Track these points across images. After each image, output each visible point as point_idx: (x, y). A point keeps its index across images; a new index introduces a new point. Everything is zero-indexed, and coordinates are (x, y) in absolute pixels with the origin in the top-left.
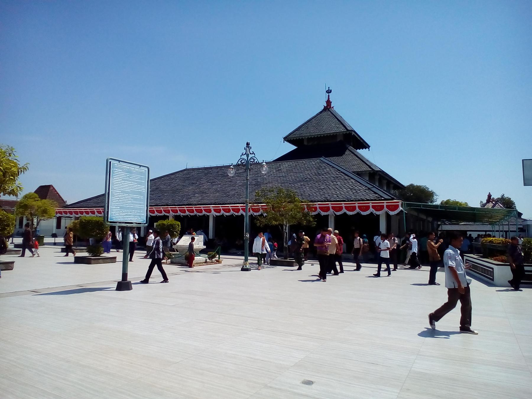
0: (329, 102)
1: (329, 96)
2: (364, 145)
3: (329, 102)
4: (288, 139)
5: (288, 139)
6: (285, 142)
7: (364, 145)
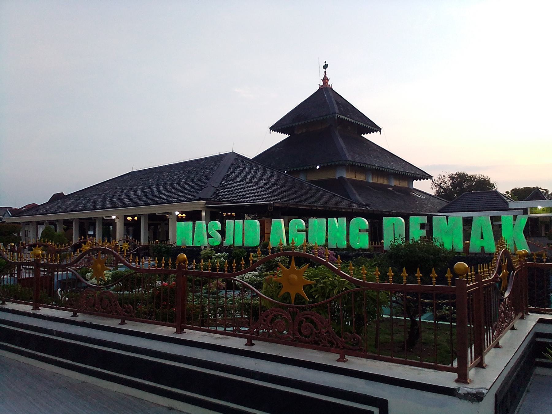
4: (277, 128)
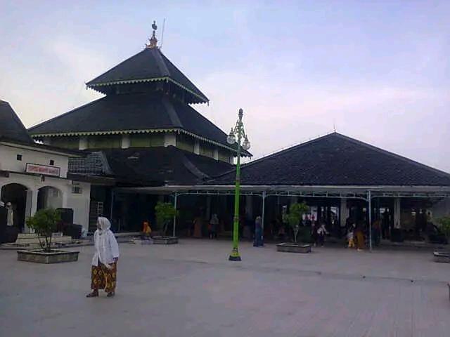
0: (154, 41)
1: (154, 32)
2: (202, 99)
3: (154, 41)
4: (94, 84)
5: (94, 84)
6: (90, 89)
7: (202, 99)
